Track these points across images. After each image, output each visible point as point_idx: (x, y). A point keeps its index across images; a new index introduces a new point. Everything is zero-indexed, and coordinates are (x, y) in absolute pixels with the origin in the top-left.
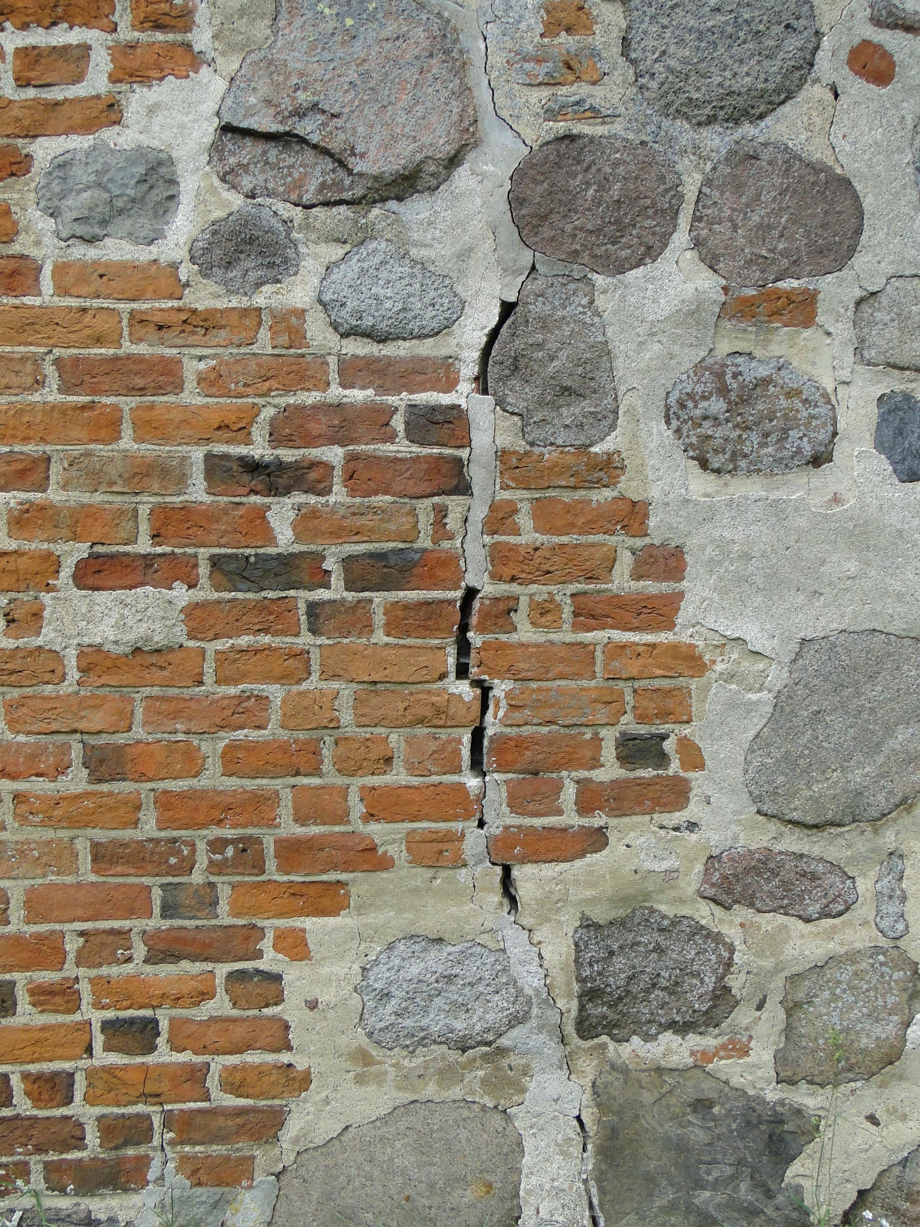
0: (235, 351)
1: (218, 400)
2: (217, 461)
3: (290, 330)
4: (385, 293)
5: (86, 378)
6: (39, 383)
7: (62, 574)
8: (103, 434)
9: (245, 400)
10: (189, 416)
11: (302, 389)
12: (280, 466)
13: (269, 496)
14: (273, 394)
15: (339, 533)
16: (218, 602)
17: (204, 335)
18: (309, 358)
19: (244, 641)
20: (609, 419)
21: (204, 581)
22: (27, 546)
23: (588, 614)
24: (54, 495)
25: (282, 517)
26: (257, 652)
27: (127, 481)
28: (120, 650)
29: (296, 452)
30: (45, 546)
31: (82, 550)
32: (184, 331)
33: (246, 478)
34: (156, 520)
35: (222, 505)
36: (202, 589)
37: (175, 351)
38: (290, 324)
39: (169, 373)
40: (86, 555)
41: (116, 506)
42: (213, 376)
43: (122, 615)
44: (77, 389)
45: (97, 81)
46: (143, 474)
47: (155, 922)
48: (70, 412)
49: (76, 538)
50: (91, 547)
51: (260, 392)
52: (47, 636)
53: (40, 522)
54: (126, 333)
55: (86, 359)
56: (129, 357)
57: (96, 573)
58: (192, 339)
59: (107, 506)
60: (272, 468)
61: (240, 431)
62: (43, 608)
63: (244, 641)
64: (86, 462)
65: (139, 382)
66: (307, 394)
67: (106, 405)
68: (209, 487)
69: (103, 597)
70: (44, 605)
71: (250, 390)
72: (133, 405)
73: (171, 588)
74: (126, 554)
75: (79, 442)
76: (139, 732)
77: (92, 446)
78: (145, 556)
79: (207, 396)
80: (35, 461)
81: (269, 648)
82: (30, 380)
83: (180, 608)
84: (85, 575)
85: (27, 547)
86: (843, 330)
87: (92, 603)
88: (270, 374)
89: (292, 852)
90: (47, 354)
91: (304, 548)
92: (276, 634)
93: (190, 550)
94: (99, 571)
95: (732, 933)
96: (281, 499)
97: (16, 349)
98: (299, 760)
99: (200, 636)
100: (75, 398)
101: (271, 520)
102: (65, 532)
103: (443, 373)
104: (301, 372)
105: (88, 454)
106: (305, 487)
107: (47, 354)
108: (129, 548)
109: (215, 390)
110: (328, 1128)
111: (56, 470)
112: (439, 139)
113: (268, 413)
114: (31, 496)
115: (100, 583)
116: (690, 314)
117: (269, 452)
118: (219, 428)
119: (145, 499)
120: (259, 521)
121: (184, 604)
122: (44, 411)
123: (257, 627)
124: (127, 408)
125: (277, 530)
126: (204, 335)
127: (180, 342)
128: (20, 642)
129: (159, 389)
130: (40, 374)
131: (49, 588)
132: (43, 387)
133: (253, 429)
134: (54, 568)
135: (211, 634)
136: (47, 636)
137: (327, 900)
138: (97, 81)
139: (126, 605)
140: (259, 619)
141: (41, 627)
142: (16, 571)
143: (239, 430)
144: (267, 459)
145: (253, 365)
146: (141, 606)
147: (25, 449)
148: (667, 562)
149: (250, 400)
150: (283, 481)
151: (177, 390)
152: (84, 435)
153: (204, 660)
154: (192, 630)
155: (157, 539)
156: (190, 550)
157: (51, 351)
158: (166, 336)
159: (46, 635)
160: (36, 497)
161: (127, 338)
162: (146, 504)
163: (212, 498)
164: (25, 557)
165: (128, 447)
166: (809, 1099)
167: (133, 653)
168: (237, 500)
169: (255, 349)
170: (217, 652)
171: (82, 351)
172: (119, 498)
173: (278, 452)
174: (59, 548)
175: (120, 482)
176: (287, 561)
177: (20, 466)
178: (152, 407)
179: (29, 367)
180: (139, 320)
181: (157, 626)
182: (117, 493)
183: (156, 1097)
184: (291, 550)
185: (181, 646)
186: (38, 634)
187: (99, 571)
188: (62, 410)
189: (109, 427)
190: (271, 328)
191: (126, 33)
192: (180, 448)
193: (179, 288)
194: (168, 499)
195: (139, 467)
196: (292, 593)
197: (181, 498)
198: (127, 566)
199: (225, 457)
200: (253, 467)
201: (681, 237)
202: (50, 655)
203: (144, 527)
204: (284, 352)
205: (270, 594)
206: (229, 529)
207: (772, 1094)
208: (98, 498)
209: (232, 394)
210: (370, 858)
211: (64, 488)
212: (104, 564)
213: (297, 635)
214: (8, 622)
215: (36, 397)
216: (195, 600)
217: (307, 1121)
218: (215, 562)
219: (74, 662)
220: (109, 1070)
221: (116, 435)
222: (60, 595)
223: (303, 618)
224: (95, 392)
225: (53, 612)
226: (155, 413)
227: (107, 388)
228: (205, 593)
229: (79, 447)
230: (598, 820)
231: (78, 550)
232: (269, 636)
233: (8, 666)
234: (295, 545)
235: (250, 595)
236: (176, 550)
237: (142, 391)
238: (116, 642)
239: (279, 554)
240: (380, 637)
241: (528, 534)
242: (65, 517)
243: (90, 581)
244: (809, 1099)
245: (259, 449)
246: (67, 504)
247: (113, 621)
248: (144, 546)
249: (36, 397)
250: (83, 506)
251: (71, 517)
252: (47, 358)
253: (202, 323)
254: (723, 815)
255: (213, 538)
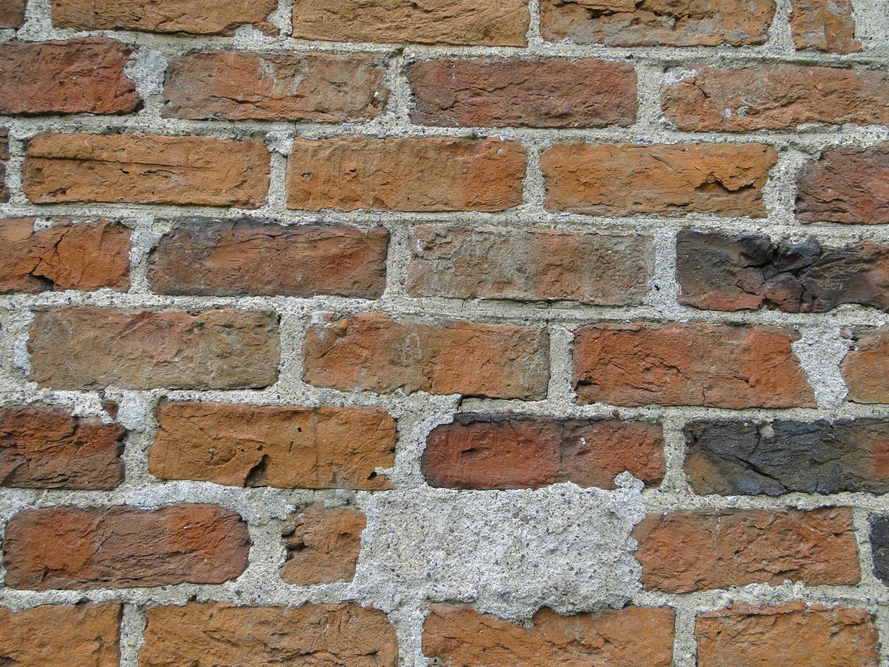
0: (730, 54)
1: (701, 136)
2: (699, 245)
3: (827, 21)
5: (461, 96)
6: (378, 104)
7: (401, 455)
8: (490, 194)
9: (750, 138)
10: (650, 165)
11: (853, 121)
12: (819, 258)
13: (797, 311)
14: (801, 127)
16: (703, 515)
17: (674, 28)
18: (859, 70)
19: (752, 594)
21: (674, 473)
22: (338, 399)
24: (394, 303)
26: (779, 616)
27: (533, 280)
28: (512, 611)
29: (847, 231)
30: (372, 400)
31: (442, 408)
32: (636, 21)
33: (754, 277)
34: (587, 354)
35: (711, 328)
36: (672, 488)
37: (622, 53)
39: (613, 89)
40: (448, 419)
41: (507, 326)
42: (692, 95)
43: (518, 540)
44: (446, 114)
46: (561, 268)
48: (431, 154)
49: (430, 385)
50: (460, 403)
51: (778, 124)
52: (367, 580)
53: (365, 353)
54: (535, 23)
55: (465, 64)
56: (541, 62)
57: (469, 454)
58: (652, 35)
59: (491, 325)
60: (807, 259)
62: (360, 522)
63: (752, 594)
64: (457, 244)
65: (560, 105)
66: (862, 129)
67: (496, 142)
68: (686, 293)
69: (479, 502)
70: (362, 516)
71: (759, 121)
72: (546, 143)
73: (612, 487)
74: (526, 418)
75: (448, 207)
77: (469, 215)
78: (562, 423)
79: (681, 129)
80: (362, 240)
81: (801, 610)
82: (361, 98)
83: (629, 526)
84: (445, 458)
85: (338, 401)
87: (458, 514)
88: (794, 93)
90: (393, 55)
91: (865, 412)
92: (813, 581)
93: (650, 413)
94: (472, 450)
96: (820, 317)
97: (338, 46)
99: (666, 583)
100: (441, 130)
101: (802, 357)
102: (412, 374)
105: (462, 229)
106: (865, 297)
107: (393, 55)
108: (532, 407)
109: (694, 120)
111: (397, 254)
113: (791, 162)
114: (350, 304)
115: (475, 474)
117: (799, 230)
118: (703, 187)
119: (565, 314)
120: (780, 358)
121: (637, 518)
122: (385, 153)
123: (777, 567)
124: (535, 149)
125: (814, 376)
126: (674, 28)
127: (632, 38)
128: (313, 593)
129: (594, 117)
130: (380, 87)
131: (375, 482)
132: (384, 111)
133: (767, 189)
134: (386, 443)
135: (689, 579)
136: (367, 580)
139: (526, 520)
140: (776, 553)
141: (355, 561)
142: (314, 448)
143: (742, 189)
144: (794, 242)
145: (762, 77)
146: (556, 522)
147: (344, 218)
149: (760, 138)
150: (825, 284)
151: (627, 120)
152: (457, 195)
153: (673, 633)
154: (653, 571)
155: (586, 390)
156: (650, 413)
157: (400, 52)
158: (606, 28)
159: (364, 577)
160: (362, 306)
161: (537, 30)
162: (565, 325)
163: (691, 313)
164: (333, 421)
165: (535, 217)
167: (535, 617)
168: (737, 317)
169: (765, 51)
170: (701, 618)
171: (456, 51)
172: (515, 312)
173: (813, 230)
174: (396, 404)
175: (519, 281)
176: (834, 436)
177: (334, 250)
178: (581, 146)
179: (361, 75)
181: (587, 563)
182: (514, 301)
184: (841, 415)
185: (628, 604)
186: (349, 575)
187: (472, 450)
188: (419, 151)
189: (503, 181)
190: (791, 18)
192: (631, 221)
194: (608, 314)
195: (555, 253)
196: (844, 498)
197: (633, 313)
198: (528, 441)
199: (715, 237)
200: (764, 257)
202: (371, 619)
203: (561, 368)
204: (817, 57)
205: (803, 502)
206: (724, 372)
208: (475, 310)
209: (727, 126)
211: (413, 290)
212: (484, 436)
213: (854, 584)
214: (290, 549)
215: (372, 128)
216: (657, 510)
218: (696, 436)
219: (416, 636)
221: (514, 196)
222: (396, 496)
223: (865, 549)
224: (478, 121)
225: (380, 532)
226: (586, 158)
227: (500, 113)
228: (676, 497)
229: (445, 216)
231: (435, 408)
232: (798, 586)
233: (285, 643)
234: (848, 405)
235: (763, 503)
236: (622, 411)
237: (563, 119)
238: (503, 596)
239: (820, 423)
242: (414, 344)
243: (456, 469)
245: (779, 223)
246: (418, 321)
247: (498, 551)
248: (560, 402)
249: (372, 128)
250: (448, 325)
251: (425, 345)
252: (393, 62)
255: (694, 389)
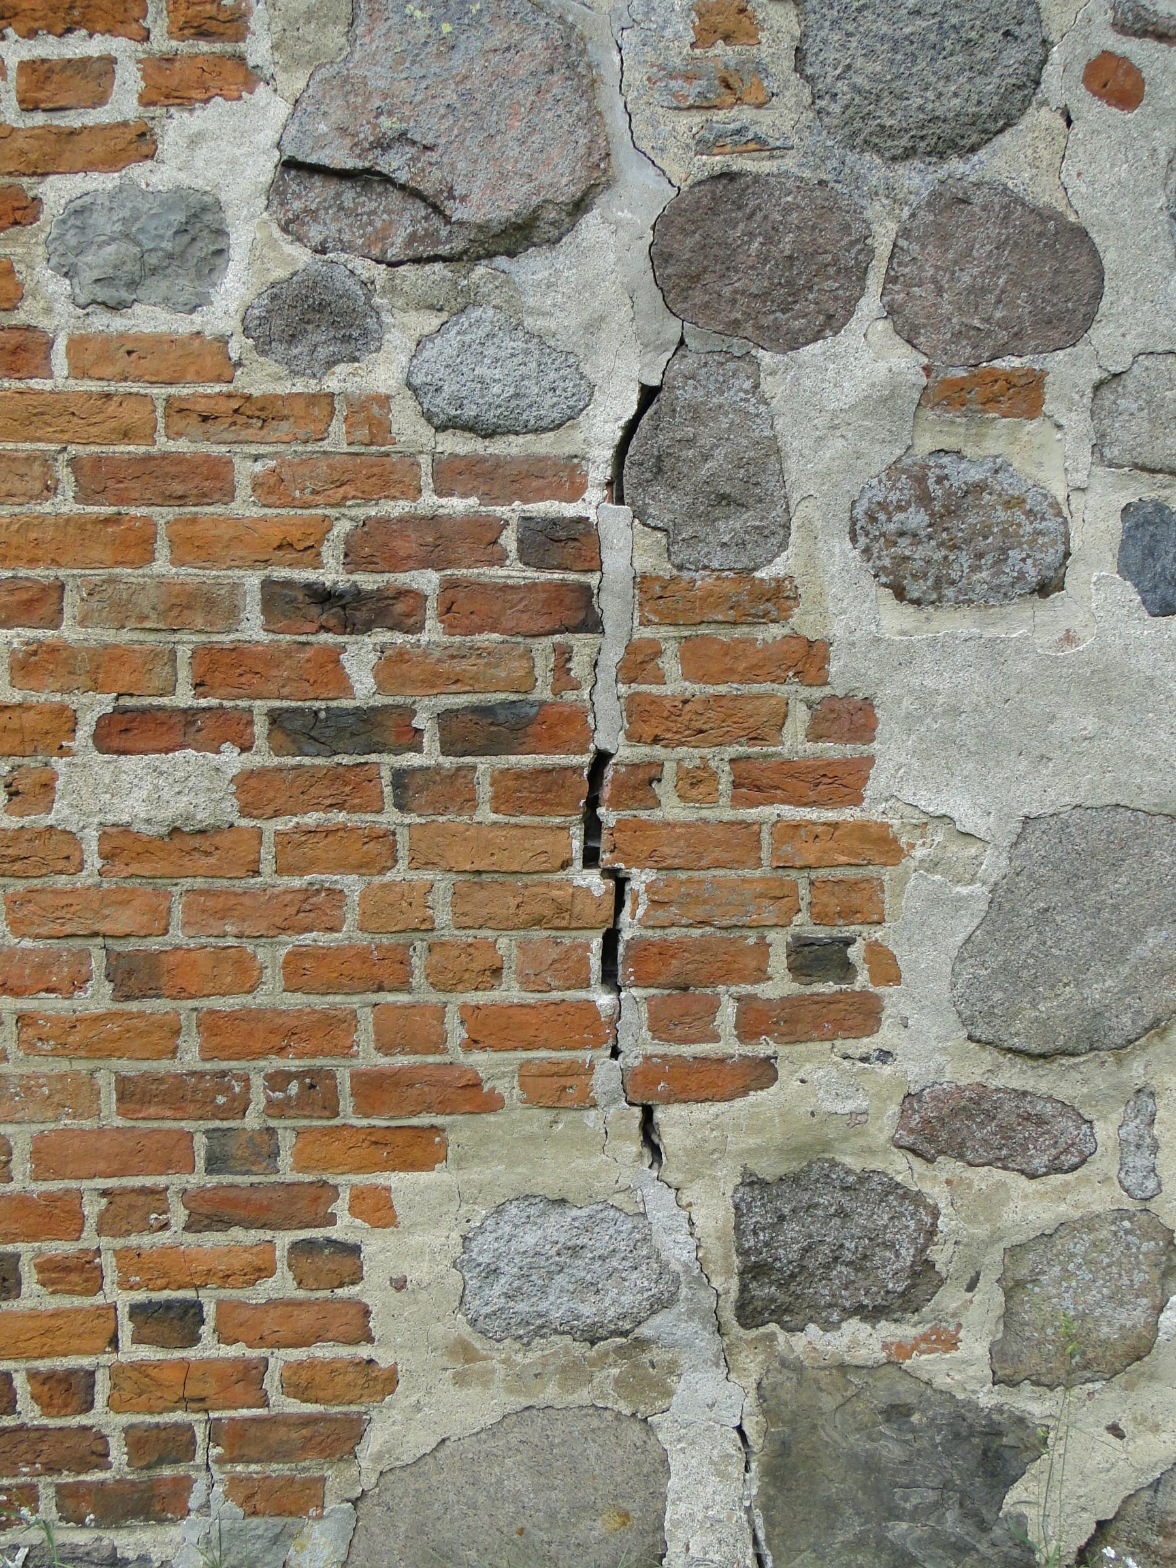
4: (493, 374)
15: (434, 681)
19: (312, 819)
20: (778, 535)
23: (752, 784)
25: (361, 661)
38: (370, 414)
45: (124, 104)
47: (198, 1179)
61: (307, 550)
63: (312, 819)
76: (177, 936)
86: (1077, 422)
89: (374, 1089)
95: (936, 1192)
98: (383, 971)
103: (566, 477)
104: (385, 475)
110: (419, 1441)
112: (561, 178)
116: (883, 402)
129: (204, 498)
137: (418, 1150)
138: (124, 104)
148: (853, 718)
162: (186, 644)
166: (1034, 1405)
180: (177, 409)
183: (199, 1402)
189: (140, 546)
191: (161, 43)
193: (228, 368)
200: (323, 597)
201: (870, 303)
207: (987, 1398)
210: (473, 1096)
217: (392, 1432)
220: (140, 1367)
228: (262, 758)
230: (764, 1048)
240: (485, 814)
241: (675, 683)
244: (1034, 1405)
245: (331, 574)
248: (184, 697)
253: (259, 413)
254: (924, 1042)
